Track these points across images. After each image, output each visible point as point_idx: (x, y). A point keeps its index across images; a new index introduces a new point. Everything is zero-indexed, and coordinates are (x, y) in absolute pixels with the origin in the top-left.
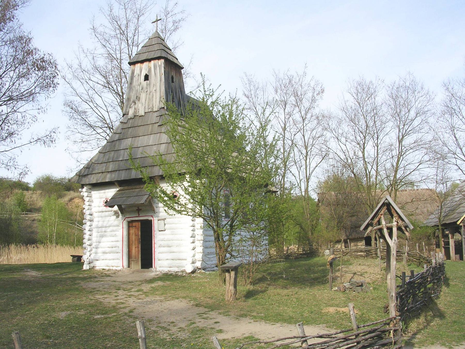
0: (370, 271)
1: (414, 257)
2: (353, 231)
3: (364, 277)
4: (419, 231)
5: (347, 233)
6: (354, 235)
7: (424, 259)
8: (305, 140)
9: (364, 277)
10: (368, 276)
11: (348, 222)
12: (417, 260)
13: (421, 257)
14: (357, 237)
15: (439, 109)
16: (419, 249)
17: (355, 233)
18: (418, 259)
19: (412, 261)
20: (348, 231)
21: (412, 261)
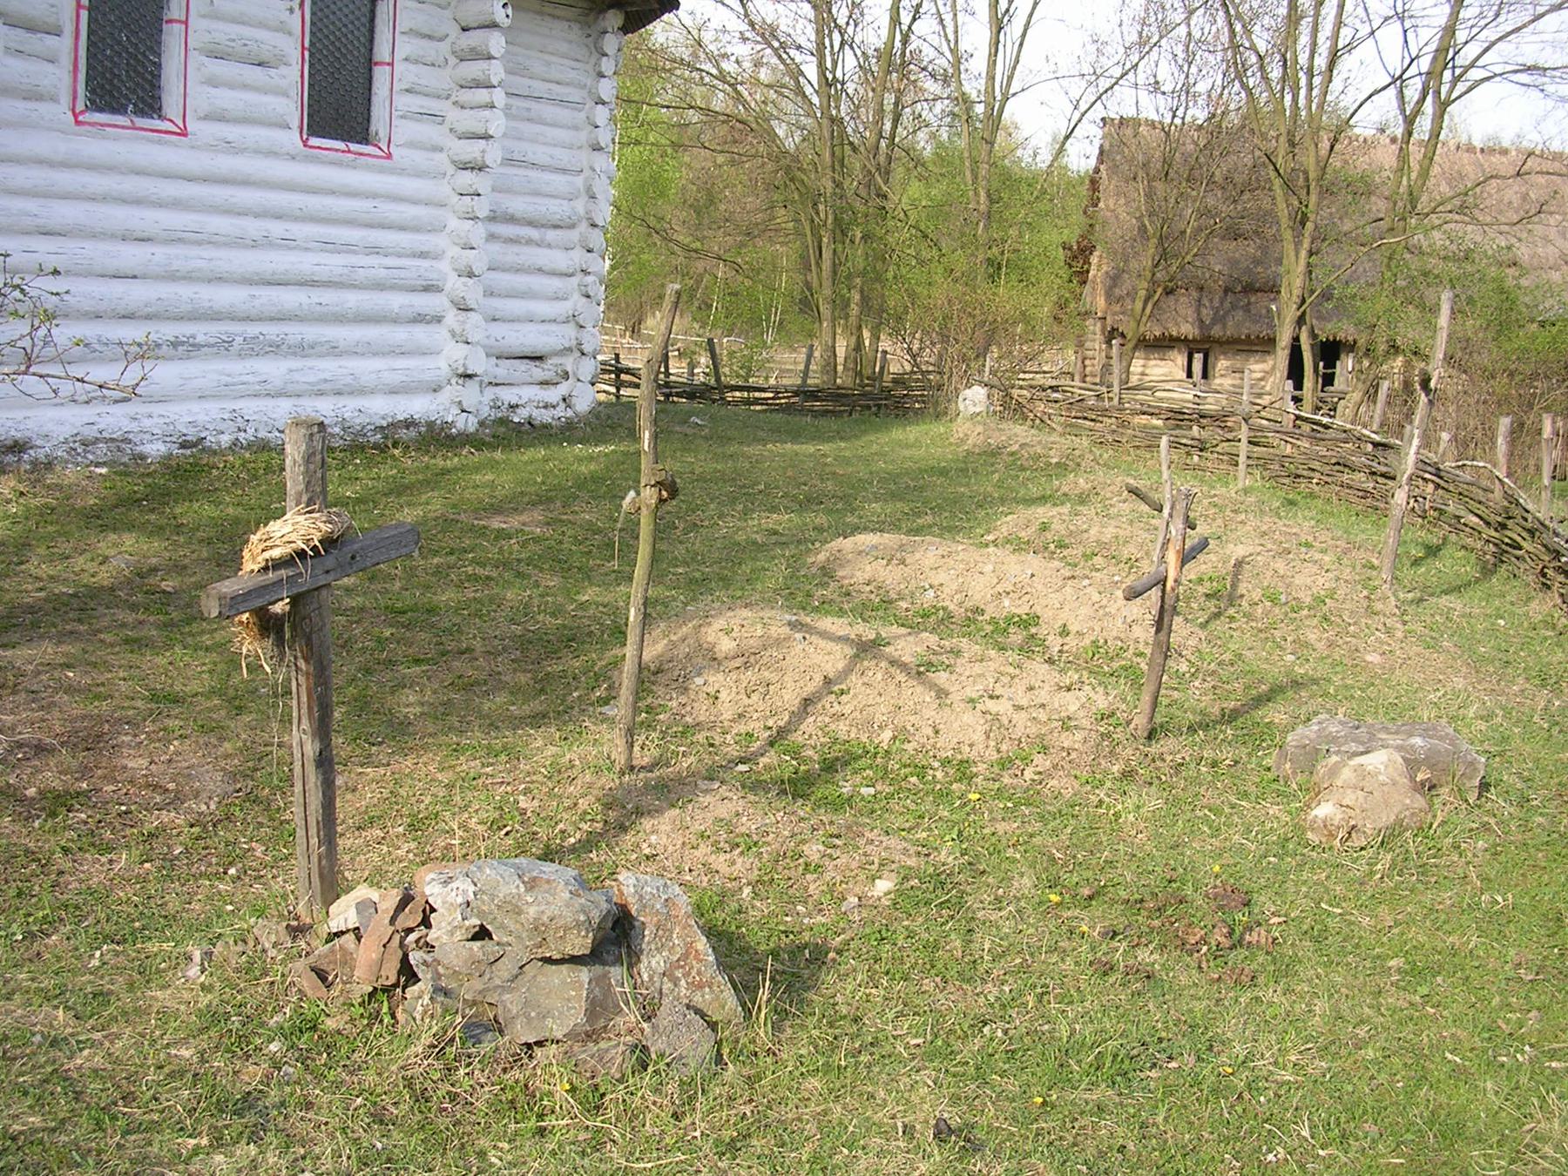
0: (1064, 616)
1: (1473, 505)
2: (1234, 307)
3: (942, 693)
4: (1534, 338)
5: (1204, 311)
6: (1237, 325)
7: (1531, 532)
8: (1356, 111)
9: (942, 693)
10: (971, 692)
11: (1220, 260)
12: (1488, 524)
13: (1517, 512)
14: (1248, 336)
15: (1420, 802)
16: (1511, 454)
17: (1239, 314)
18: (1493, 518)
19: (1457, 523)
20: (1211, 301)
21: (1457, 523)
